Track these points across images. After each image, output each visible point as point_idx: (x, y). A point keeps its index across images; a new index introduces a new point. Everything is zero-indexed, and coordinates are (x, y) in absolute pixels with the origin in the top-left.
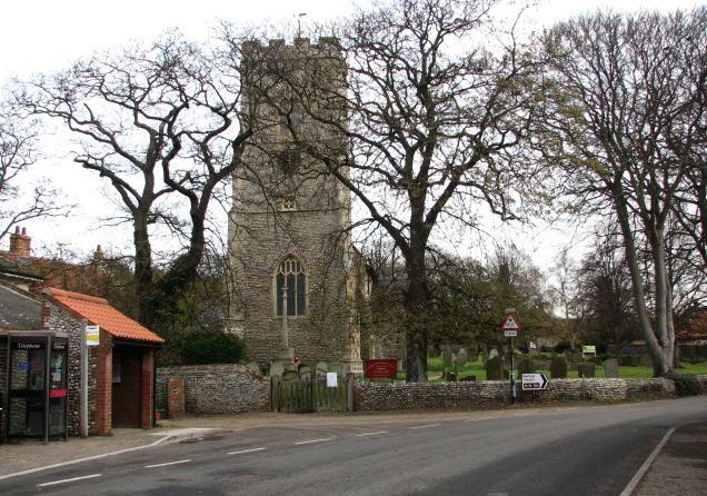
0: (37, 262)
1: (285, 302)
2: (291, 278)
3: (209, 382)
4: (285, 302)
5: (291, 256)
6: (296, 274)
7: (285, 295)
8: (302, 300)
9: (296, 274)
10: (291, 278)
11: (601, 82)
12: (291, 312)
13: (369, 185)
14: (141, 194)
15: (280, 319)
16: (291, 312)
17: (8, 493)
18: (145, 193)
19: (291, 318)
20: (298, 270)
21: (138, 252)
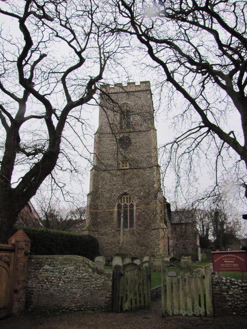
0: (34, 90)
1: (122, 219)
2: (126, 206)
3: (46, 274)
4: (122, 219)
5: (125, 194)
6: (128, 204)
7: (122, 215)
8: (132, 219)
9: (128, 204)
10: (126, 206)
11: (203, 230)
12: (125, 226)
13: (72, 32)
14: (14, 117)
15: (119, 230)
16: (125, 226)
17: (3, 114)
18: (17, 116)
19: (126, 230)
20: (130, 202)
21: (203, 119)
